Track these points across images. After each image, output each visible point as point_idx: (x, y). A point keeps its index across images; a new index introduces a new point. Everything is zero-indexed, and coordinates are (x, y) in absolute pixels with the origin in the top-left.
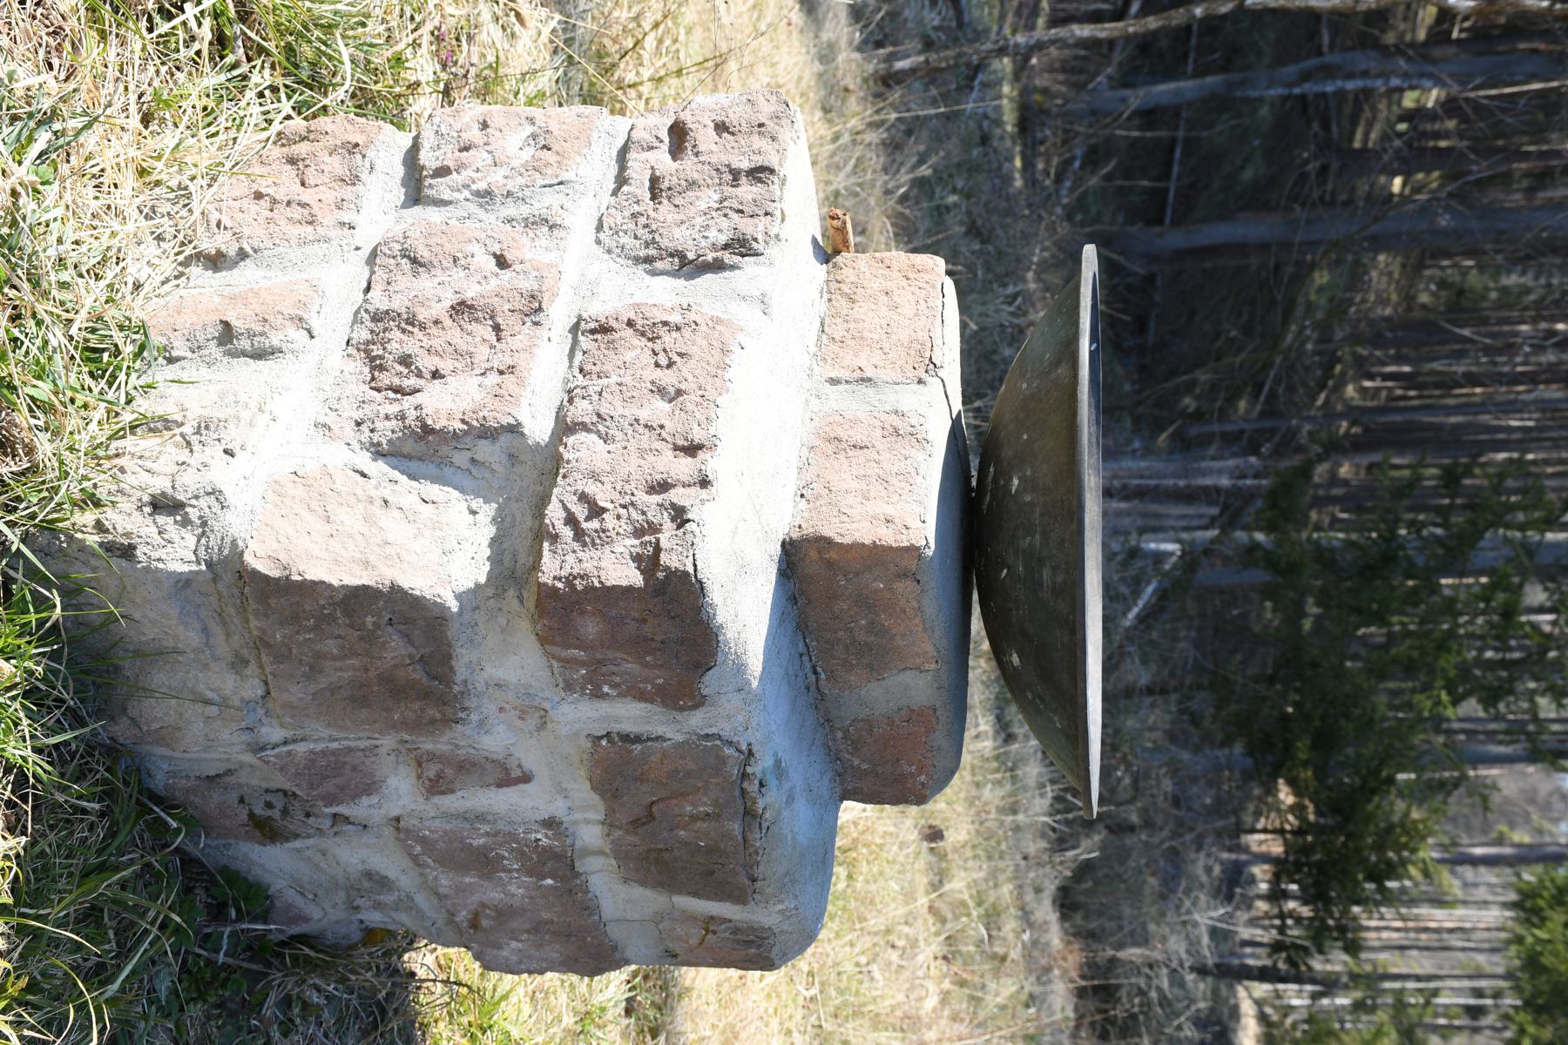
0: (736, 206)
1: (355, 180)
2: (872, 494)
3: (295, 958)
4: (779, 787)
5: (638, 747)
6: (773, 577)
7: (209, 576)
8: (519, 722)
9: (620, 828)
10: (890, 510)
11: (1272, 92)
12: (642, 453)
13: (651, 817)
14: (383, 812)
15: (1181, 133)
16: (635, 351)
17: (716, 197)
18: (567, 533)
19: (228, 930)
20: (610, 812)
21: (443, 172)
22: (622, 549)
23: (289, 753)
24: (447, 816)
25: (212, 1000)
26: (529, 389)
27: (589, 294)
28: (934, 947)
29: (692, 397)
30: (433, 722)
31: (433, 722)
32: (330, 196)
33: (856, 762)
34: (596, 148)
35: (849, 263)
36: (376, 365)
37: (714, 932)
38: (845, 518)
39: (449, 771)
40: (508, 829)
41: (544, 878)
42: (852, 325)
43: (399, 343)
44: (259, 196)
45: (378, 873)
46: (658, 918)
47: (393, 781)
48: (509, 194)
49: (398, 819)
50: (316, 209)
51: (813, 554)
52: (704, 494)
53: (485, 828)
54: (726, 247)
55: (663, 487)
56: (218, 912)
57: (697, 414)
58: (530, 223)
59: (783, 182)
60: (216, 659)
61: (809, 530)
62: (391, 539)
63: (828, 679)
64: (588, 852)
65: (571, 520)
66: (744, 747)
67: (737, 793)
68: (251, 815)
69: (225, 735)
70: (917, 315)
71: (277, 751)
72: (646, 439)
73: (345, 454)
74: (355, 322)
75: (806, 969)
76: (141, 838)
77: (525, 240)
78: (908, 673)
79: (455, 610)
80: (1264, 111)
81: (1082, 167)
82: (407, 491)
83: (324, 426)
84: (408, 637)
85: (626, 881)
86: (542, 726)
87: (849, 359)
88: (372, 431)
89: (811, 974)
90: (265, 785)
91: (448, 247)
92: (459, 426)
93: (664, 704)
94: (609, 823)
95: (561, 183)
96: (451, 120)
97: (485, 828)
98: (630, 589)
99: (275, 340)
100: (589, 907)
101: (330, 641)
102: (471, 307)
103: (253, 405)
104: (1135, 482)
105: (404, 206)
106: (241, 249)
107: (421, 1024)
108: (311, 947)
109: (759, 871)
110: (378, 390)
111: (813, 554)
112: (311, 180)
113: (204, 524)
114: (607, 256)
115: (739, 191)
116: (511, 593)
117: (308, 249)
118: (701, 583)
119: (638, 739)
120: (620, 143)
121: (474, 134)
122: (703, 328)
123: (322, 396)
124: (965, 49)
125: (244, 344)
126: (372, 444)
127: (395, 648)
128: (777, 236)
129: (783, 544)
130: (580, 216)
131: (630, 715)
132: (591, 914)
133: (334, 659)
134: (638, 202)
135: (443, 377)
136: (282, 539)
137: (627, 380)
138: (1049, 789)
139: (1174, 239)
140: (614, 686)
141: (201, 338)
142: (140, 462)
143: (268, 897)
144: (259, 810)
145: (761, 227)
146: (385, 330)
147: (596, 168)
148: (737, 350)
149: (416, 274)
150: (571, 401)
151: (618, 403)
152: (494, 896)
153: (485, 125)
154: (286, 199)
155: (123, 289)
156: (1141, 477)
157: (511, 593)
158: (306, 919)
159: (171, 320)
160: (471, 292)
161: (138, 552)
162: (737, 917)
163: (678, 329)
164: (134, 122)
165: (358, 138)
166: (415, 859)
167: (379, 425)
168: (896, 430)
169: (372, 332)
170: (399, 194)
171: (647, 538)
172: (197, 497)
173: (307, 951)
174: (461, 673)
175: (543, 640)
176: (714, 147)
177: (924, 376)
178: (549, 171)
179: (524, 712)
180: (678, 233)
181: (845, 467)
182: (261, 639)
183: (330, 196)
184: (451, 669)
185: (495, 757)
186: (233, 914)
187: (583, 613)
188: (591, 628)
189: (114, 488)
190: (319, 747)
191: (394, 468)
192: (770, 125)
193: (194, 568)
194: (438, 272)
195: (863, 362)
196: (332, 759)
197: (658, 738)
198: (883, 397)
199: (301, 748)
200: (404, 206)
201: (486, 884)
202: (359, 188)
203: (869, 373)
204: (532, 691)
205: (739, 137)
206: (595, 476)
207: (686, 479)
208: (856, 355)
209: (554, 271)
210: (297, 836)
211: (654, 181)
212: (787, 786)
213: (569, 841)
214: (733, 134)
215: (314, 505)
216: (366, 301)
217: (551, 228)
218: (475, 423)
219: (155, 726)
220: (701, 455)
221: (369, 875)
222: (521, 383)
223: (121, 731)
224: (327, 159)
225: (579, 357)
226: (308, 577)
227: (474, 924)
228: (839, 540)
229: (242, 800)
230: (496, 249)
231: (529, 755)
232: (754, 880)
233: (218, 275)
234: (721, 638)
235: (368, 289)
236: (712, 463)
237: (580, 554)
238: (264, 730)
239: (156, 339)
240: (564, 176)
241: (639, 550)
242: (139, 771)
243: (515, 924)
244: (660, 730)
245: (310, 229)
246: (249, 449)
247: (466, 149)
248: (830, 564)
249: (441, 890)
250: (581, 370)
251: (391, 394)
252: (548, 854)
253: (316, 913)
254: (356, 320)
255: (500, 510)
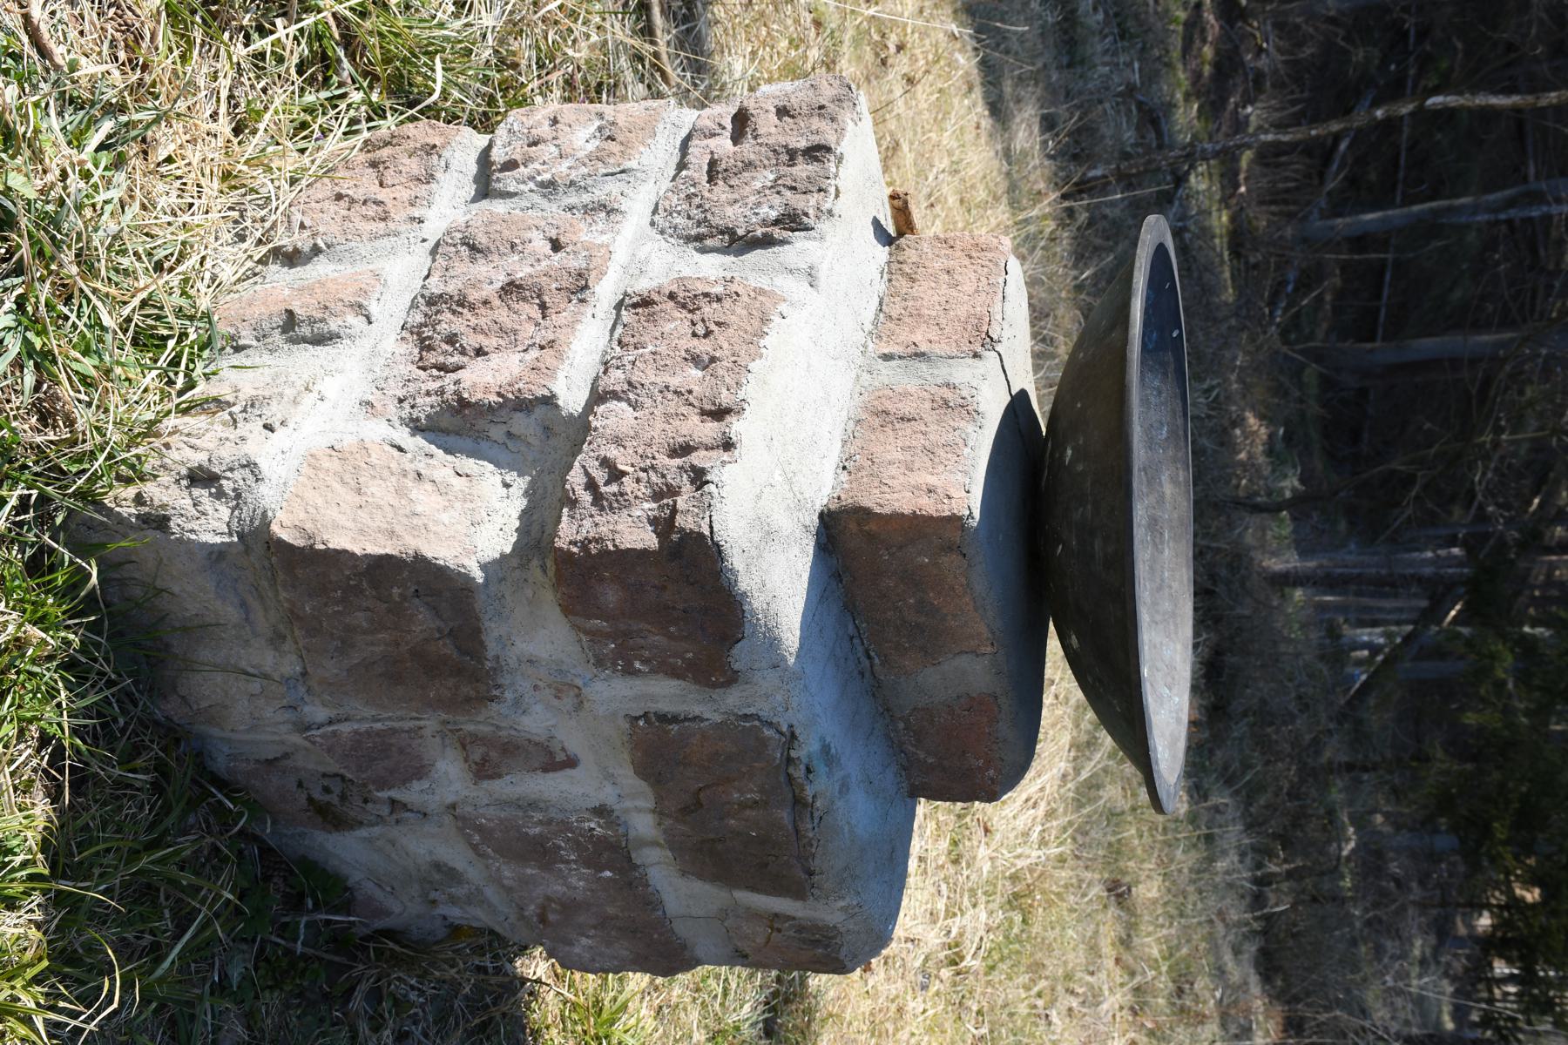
0: (789, 183)
1: (430, 178)
2: (916, 466)
3: (380, 953)
4: (829, 775)
5: (675, 727)
6: (811, 550)
7: (241, 548)
8: (556, 702)
9: (669, 816)
10: (932, 480)
11: (1479, 218)
12: (668, 417)
13: (699, 804)
14: (437, 798)
15: (1390, 256)
16: (676, 324)
17: (772, 177)
18: (587, 498)
19: (304, 919)
20: (659, 799)
21: (511, 165)
22: (639, 513)
23: (334, 733)
24: (503, 803)
25: (287, 988)
26: (567, 362)
27: (638, 272)
28: (1118, 996)
29: (725, 363)
30: (468, 700)
31: (468, 700)
32: (404, 194)
33: (922, 755)
34: (661, 139)
35: (912, 244)
36: (425, 345)
37: (779, 931)
38: (886, 489)
39: (493, 754)
40: (560, 816)
41: (602, 870)
42: (910, 304)
43: (448, 323)
44: (339, 197)
45: (445, 865)
46: (723, 915)
47: (442, 766)
48: (572, 183)
49: (453, 806)
50: (390, 205)
51: (853, 526)
52: (726, 457)
53: (538, 816)
54: (776, 222)
55: (684, 450)
56: (295, 903)
57: (727, 380)
58: (589, 210)
59: (840, 159)
60: (255, 634)
61: (848, 501)
62: (419, 509)
63: (883, 664)
64: (644, 843)
65: (591, 485)
66: (784, 729)
67: (782, 779)
68: (310, 800)
69: (268, 713)
70: (977, 291)
71: (321, 731)
72: (674, 405)
73: (381, 430)
74: (411, 307)
75: (975, 1008)
76: (207, 821)
77: (582, 225)
78: (964, 657)
79: (481, 581)
80: (1471, 237)
81: (1296, 289)
82: (442, 465)
83: (368, 403)
84: (436, 611)
85: (684, 873)
86: (579, 706)
87: (904, 335)
88: (412, 407)
89: (979, 1013)
90: (322, 769)
91: (506, 233)
92: (494, 398)
93: (697, 681)
94: (659, 812)
95: (623, 172)
96: (524, 119)
97: (538, 816)
98: (644, 553)
99: (333, 325)
100: (651, 902)
101: (359, 614)
102: (519, 287)
103: (300, 384)
104: (1339, 571)
105: (474, 200)
106: (315, 245)
107: (532, 1030)
108: (397, 942)
109: (816, 864)
110: (424, 369)
111: (853, 526)
112: (389, 181)
113: (238, 496)
114: (659, 237)
115: (794, 170)
116: (535, 563)
117: (378, 243)
118: (718, 545)
119: (675, 719)
120: (684, 133)
121: (545, 130)
122: (745, 298)
123: (370, 377)
124: (1153, 156)
125: (305, 331)
126: (412, 420)
127: (423, 622)
128: (830, 212)
129: (821, 515)
130: (638, 203)
131: (666, 693)
132: (654, 909)
133: (365, 632)
134: (694, 185)
135: (486, 354)
136: (311, 510)
137: (663, 349)
138: (1249, 857)
139: (1381, 352)
140: (645, 662)
141: (266, 325)
142: (186, 439)
143: (347, 889)
144: (317, 795)
145: (813, 202)
146: (438, 312)
147: (657, 156)
148: (777, 319)
149: (473, 260)
150: (605, 372)
151: (651, 372)
152: (558, 888)
153: (555, 121)
154: (362, 199)
155: (199, 284)
156: (1346, 566)
157: (535, 563)
158: (389, 913)
159: (241, 311)
160: (522, 272)
161: (172, 524)
162: (799, 914)
163: (719, 300)
164: (224, 126)
165: (437, 141)
166: (475, 848)
167: (419, 401)
168: (946, 402)
169: (426, 315)
170: (470, 190)
171: (665, 501)
172: (231, 470)
173: (391, 945)
174: (492, 648)
175: (567, 611)
176: (773, 130)
177: (979, 350)
178: (612, 161)
179: (559, 691)
180: (729, 211)
181: (891, 439)
182: (292, 612)
183: (404, 194)
184: (482, 643)
185: (537, 739)
186: (310, 903)
187: (602, 580)
188: (611, 596)
189: (159, 463)
190: (364, 727)
191: (430, 443)
192: (831, 107)
193: (227, 539)
194: (495, 257)
195: (918, 338)
196: (377, 740)
197: (695, 718)
198: (936, 372)
199: (345, 728)
200: (474, 200)
201: (547, 876)
202: (434, 186)
203: (923, 348)
204: (564, 668)
205: (799, 120)
206: (618, 441)
207: (709, 441)
208: (912, 332)
209: (603, 251)
210: (361, 824)
211: (713, 164)
212: (839, 774)
213: (621, 830)
214: (793, 117)
215: (347, 478)
216: (423, 287)
217: (608, 213)
218: (510, 396)
219: (204, 704)
220: (728, 419)
221: (438, 866)
222: (560, 357)
223: (171, 708)
224: (406, 161)
225: (619, 330)
226: (331, 546)
227: (543, 919)
228: (878, 510)
229: (300, 785)
230: (553, 234)
231: (572, 738)
232: (811, 874)
233: (294, 270)
234: (746, 607)
235: (427, 277)
236: (737, 427)
237: (598, 518)
238: (307, 709)
239: (223, 328)
240: (627, 165)
241: (656, 513)
242: (200, 758)
243: (581, 918)
244: (697, 710)
245: (382, 225)
246: (291, 425)
247: (535, 144)
248: (871, 537)
249: (506, 882)
250: (620, 342)
251: (435, 372)
252: (602, 844)
253: (396, 908)
254: (414, 305)
255: (532, 484)
